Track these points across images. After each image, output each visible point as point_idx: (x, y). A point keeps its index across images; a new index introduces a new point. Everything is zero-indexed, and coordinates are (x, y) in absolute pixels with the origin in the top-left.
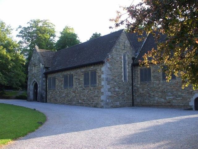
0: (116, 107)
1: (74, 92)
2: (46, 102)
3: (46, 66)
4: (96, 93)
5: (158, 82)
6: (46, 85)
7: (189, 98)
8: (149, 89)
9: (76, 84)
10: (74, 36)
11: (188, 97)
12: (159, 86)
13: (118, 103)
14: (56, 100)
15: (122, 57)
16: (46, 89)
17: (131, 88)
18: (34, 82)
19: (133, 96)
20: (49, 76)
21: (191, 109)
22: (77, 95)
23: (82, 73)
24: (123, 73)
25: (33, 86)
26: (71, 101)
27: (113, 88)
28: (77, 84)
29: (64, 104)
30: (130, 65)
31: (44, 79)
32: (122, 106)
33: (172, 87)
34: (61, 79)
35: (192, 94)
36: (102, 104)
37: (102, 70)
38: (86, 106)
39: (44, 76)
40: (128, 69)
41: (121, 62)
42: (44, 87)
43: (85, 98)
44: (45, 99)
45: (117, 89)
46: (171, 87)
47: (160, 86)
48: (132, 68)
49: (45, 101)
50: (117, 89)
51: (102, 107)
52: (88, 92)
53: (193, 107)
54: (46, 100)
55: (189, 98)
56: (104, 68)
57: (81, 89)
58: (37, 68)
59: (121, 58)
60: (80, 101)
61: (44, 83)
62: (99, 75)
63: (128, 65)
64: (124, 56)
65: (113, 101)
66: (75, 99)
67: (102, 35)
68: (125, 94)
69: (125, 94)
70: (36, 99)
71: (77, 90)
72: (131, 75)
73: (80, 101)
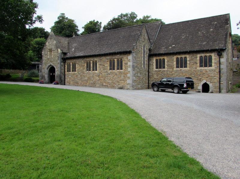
0: (139, 89)
1: (99, 76)
2: (65, 85)
3: (64, 51)
4: (122, 77)
5: (171, 70)
6: (65, 69)
7: (197, 83)
8: (163, 75)
9: (100, 70)
10: (44, 29)
11: (197, 82)
12: (172, 73)
13: (139, 86)
14: (77, 83)
15: (143, 48)
16: (65, 73)
17: (147, 74)
18: (49, 66)
19: (149, 80)
20: (67, 61)
21: (199, 92)
22: (102, 78)
23: (108, 60)
24: (143, 62)
25: (48, 70)
26: (94, 84)
27: (137, 73)
28: (102, 69)
29: (86, 86)
30: (147, 55)
31: (62, 64)
32: (142, 88)
33: (184, 74)
34: (83, 64)
35: (200, 80)
36: (128, 86)
37: (129, 58)
38: (111, 88)
39: (62, 60)
40: (146, 59)
41: (142, 52)
42: (63, 71)
43: (111, 82)
44: (63, 82)
45: (139, 75)
46: (182, 74)
47: (173, 73)
48: (149, 58)
49: (63, 83)
50: (139, 75)
51: (128, 89)
52: (114, 76)
53: (201, 90)
54: (65, 83)
55: (197, 83)
56: (130, 57)
57: (106, 73)
58: (54, 53)
59: (142, 49)
60: (104, 84)
61: (63, 68)
62: (126, 62)
63: (146, 55)
64: (144, 47)
65: (137, 84)
66: (99, 82)
67: (166, 23)
68: (144, 78)
69: (144, 78)
70: (52, 80)
71: (101, 75)
72: (148, 64)
73: (104, 84)
